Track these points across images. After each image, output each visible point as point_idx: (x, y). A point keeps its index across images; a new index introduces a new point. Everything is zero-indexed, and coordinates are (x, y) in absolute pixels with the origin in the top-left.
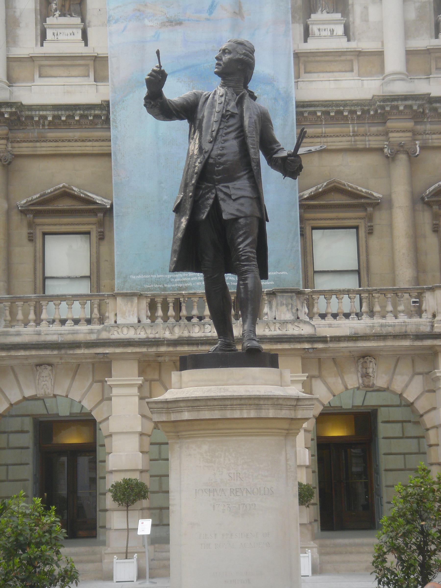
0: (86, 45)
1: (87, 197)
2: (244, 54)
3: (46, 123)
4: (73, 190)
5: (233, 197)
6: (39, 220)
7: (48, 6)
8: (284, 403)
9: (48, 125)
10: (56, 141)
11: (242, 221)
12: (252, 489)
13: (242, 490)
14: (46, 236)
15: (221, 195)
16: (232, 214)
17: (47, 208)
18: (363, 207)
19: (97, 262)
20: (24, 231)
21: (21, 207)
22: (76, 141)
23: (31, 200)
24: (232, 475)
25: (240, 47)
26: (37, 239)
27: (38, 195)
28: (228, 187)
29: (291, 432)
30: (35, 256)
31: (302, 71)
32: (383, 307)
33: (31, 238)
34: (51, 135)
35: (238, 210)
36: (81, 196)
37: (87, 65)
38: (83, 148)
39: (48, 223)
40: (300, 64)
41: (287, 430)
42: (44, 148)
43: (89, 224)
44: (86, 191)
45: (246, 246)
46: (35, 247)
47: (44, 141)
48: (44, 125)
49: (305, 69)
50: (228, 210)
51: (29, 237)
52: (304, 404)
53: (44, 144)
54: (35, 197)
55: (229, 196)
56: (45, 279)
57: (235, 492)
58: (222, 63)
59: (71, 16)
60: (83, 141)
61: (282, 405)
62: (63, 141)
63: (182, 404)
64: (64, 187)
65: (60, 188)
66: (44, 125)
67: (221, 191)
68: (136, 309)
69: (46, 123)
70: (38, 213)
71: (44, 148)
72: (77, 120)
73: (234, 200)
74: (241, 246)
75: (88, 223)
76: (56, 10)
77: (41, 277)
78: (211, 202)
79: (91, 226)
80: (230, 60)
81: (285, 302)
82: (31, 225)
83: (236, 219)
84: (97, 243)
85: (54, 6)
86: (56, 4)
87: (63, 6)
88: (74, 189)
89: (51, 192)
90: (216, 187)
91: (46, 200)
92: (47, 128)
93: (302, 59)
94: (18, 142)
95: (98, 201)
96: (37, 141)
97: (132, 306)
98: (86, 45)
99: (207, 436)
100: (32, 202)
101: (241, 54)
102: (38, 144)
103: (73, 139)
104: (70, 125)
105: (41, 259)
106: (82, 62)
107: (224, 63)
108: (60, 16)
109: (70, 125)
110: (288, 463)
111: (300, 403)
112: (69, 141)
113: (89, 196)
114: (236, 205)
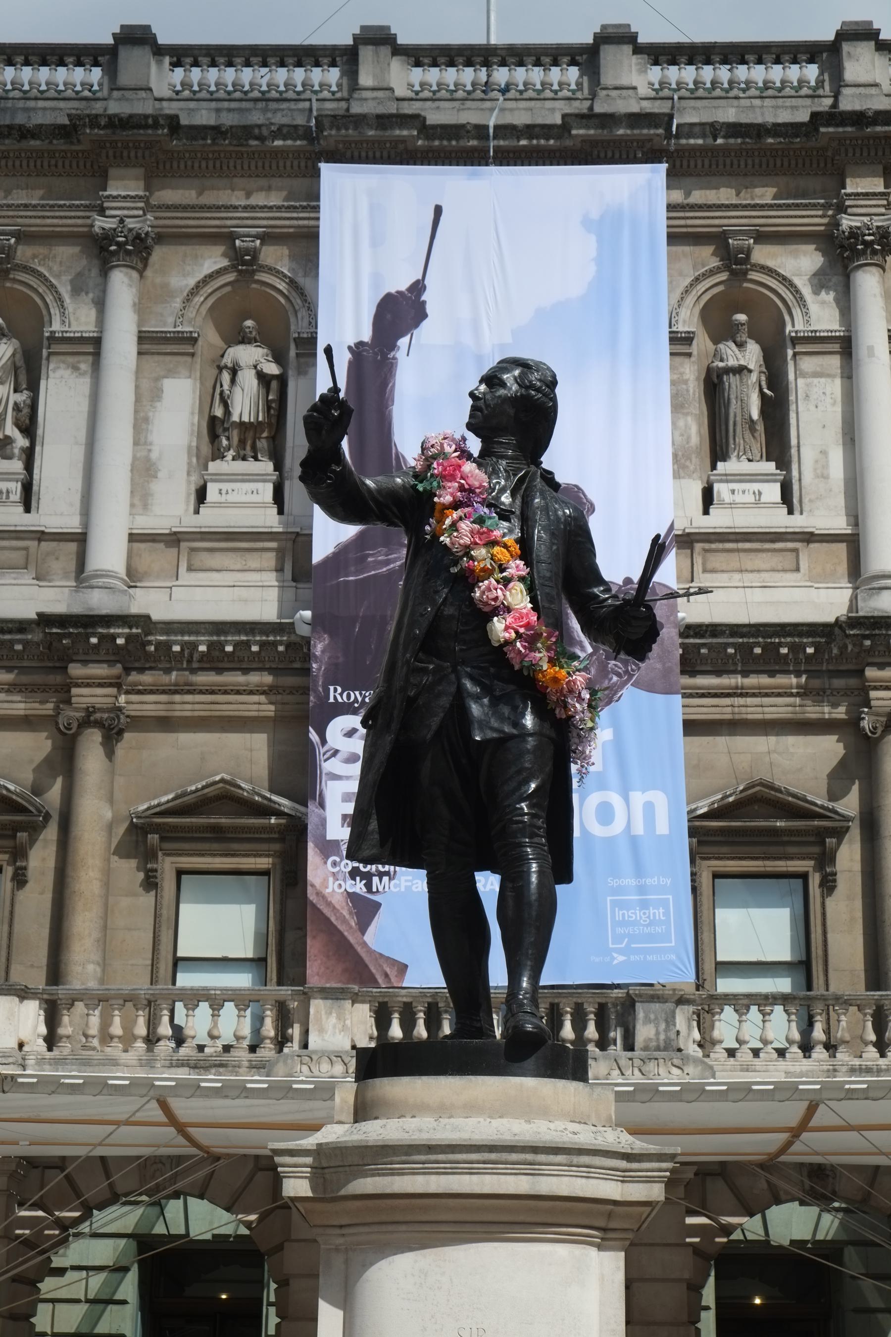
1: (265, 802)
4: (240, 787)
10: (212, 692)
17: (194, 820)
21: (138, 817)
22: (251, 693)
23: (159, 805)
27: (171, 796)
31: (698, 568)
48: (190, 661)
49: (704, 564)
53: (189, 698)
54: (164, 799)
59: (256, 459)
64: (222, 780)
66: (190, 661)
69: (196, 657)
70: (169, 835)
71: (187, 705)
89: (197, 790)
92: (195, 665)
102: (177, 698)
105: (166, 925)
112: (238, 692)
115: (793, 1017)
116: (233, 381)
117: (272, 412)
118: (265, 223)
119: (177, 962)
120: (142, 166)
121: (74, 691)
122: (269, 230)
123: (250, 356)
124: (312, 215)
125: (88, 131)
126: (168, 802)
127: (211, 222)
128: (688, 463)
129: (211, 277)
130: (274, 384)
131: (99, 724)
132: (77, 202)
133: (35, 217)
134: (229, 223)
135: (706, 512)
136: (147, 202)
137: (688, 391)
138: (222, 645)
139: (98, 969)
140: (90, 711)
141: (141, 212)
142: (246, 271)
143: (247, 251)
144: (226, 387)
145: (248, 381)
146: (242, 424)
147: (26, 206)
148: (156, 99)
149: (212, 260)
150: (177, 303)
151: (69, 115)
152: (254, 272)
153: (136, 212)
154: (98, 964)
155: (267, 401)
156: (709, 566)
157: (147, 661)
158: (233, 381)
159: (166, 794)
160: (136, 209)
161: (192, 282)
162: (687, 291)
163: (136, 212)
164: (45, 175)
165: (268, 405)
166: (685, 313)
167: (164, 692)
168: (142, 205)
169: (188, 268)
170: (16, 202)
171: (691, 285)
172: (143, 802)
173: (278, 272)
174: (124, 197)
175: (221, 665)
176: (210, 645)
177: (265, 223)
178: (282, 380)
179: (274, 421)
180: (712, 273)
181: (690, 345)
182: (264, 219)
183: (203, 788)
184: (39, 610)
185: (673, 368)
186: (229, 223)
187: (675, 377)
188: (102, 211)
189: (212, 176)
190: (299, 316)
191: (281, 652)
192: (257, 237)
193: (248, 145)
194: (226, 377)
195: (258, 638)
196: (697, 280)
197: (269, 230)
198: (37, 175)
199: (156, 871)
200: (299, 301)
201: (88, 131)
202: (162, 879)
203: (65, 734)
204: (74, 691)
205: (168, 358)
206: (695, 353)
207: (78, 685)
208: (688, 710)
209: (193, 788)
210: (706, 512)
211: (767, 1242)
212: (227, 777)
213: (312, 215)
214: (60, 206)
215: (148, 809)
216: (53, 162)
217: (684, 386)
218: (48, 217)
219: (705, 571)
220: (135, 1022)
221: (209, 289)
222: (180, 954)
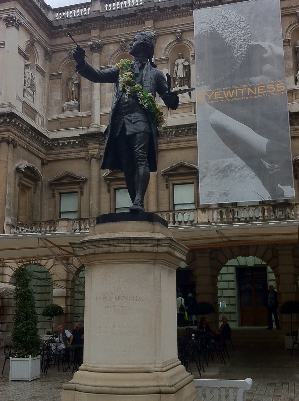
0: (191, 98)
1: (191, 166)
2: (144, 39)
3: (173, 134)
4: (185, 163)
5: (133, 122)
6: (170, 179)
7: (174, 83)
8: (148, 242)
9: (174, 135)
10: (178, 142)
11: (138, 135)
12: (129, 297)
13: (122, 298)
14: (175, 186)
15: (126, 121)
16: (131, 132)
17: (175, 172)
18: (78, 183)
19: (197, 196)
20: (165, 184)
21: (162, 173)
22: (186, 141)
23: (167, 169)
24: (116, 288)
25: (143, 36)
26: (170, 187)
27: (170, 167)
28: (130, 116)
29: (157, 261)
30: (169, 195)
31: (294, 98)
32: (85, 226)
33: (167, 187)
34: (175, 139)
35: (135, 129)
36: (188, 166)
37: (191, 107)
38: (190, 144)
39: (175, 180)
40: (293, 95)
41: (155, 260)
42: (172, 146)
43: (193, 179)
44: (191, 164)
45: (139, 150)
46: (169, 191)
47: (172, 143)
48: (172, 136)
49: (296, 97)
50: (130, 129)
51: (166, 186)
52: (163, 243)
53: (172, 144)
54: (168, 168)
55: (130, 121)
56: (174, 205)
57: (117, 299)
58: (132, 47)
59: (184, 86)
60: (189, 141)
61: (146, 243)
62: (180, 142)
63: (87, 244)
64: (181, 162)
65: (179, 163)
66: (172, 136)
67: (127, 119)
68: (207, 216)
69: (173, 134)
71: (172, 146)
72: (186, 132)
73: (134, 123)
74: (137, 150)
75: (75, 188)
76: (177, 84)
77: (172, 204)
78: (121, 126)
79: (194, 180)
80: (137, 44)
81: (281, 209)
82: (167, 181)
83: (134, 134)
84: (197, 187)
85: (177, 83)
86: (177, 82)
87: (181, 82)
88: (186, 163)
89: (175, 165)
90: (124, 117)
91: (173, 169)
92: (173, 136)
93: (294, 93)
94: (161, 144)
95: (196, 168)
96: (169, 143)
97: (205, 214)
98: (191, 98)
99: (103, 264)
100: (167, 171)
101: (142, 40)
102: (170, 144)
103: (184, 141)
104: (183, 134)
105: (172, 196)
106: (189, 106)
107: (133, 47)
108: (179, 87)
109: (183, 134)
110: (156, 281)
111: (160, 243)
112: (183, 142)
113: (193, 166)
114: (134, 126)
115: (219, 213)
116: (177, 68)
117: (187, 74)
118: (182, 28)
119: (61, 213)
120: (152, 19)
121: (89, 151)
122: (183, 30)
123: (180, 61)
124: (283, 12)
125: (139, 13)
126: (169, 168)
127: (170, 30)
128: (290, 72)
129: (170, 44)
130: (187, 67)
131: (95, 158)
132: (139, 31)
133: (130, 36)
134: (174, 30)
135: (296, 84)
136: (154, 28)
137: (289, 54)
138: (59, 143)
139: (156, 208)
140: (93, 155)
141: (153, 31)
142: (179, 41)
143: (179, 36)
144: (176, 70)
145: (181, 67)
146: (180, 78)
147: (127, 34)
148: (155, 3)
149: (171, 39)
150: (163, 51)
151: (81, 20)
152: (181, 41)
153: (152, 31)
154: (156, 207)
155: (186, 72)
156: (297, 98)
157: (162, 136)
158: (177, 68)
159: (168, 167)
160: (152, 30)
161: (166, 46)
162: (288, 29)
163: (152, 31)
164: (131, 26)
165: (186, 73)
166: (288, 35)
167: (166, 143)
168: (153, 29)
169: (165, 42)
170: (125, 33)
171: (289, 27)
172: (163, 169)
173: (186, 40)
174: (149, 28)
175: (179, 136)
176: (176, 131)
177: (182, 28)
178: (189, 66)
179: (188, 76)
180: (117, 51)
181: (290, 42)
182: (182, 27)
183: (177, 164)
184: (80, 134)
185: (284, 49)
186: (174, 30)
187: (286, 51)
188: (90, 40)
189: (169, 19)
190: (192, 50)
191: (77, 143)
192: (124, 41)
193: (176, 10)
194: (176, 67)
195: (187, 128)
196: (290, 26)
197: (183, 30)
198: (129, 26)
199: (82, 191)
200: (192, 46)
201: (139, 13)
202: (169, 186)
203: (88, 161)
204: (89, 151)
205: (162, 65)
206: (291, 44)
207: (90, 150)
208: (191, 144)
209: (174, 165)
210: (296, 84)
211: (247, 265)
212: (182, 161)
213: (283, 12)
214: (135, 32)
215: (164, 171)
216: (132, 22)
217: (288, 53)
218: (132, 35)
219: (296, 99)
220: (87, 225)
221: (170, 47)
222: (116, 207)
